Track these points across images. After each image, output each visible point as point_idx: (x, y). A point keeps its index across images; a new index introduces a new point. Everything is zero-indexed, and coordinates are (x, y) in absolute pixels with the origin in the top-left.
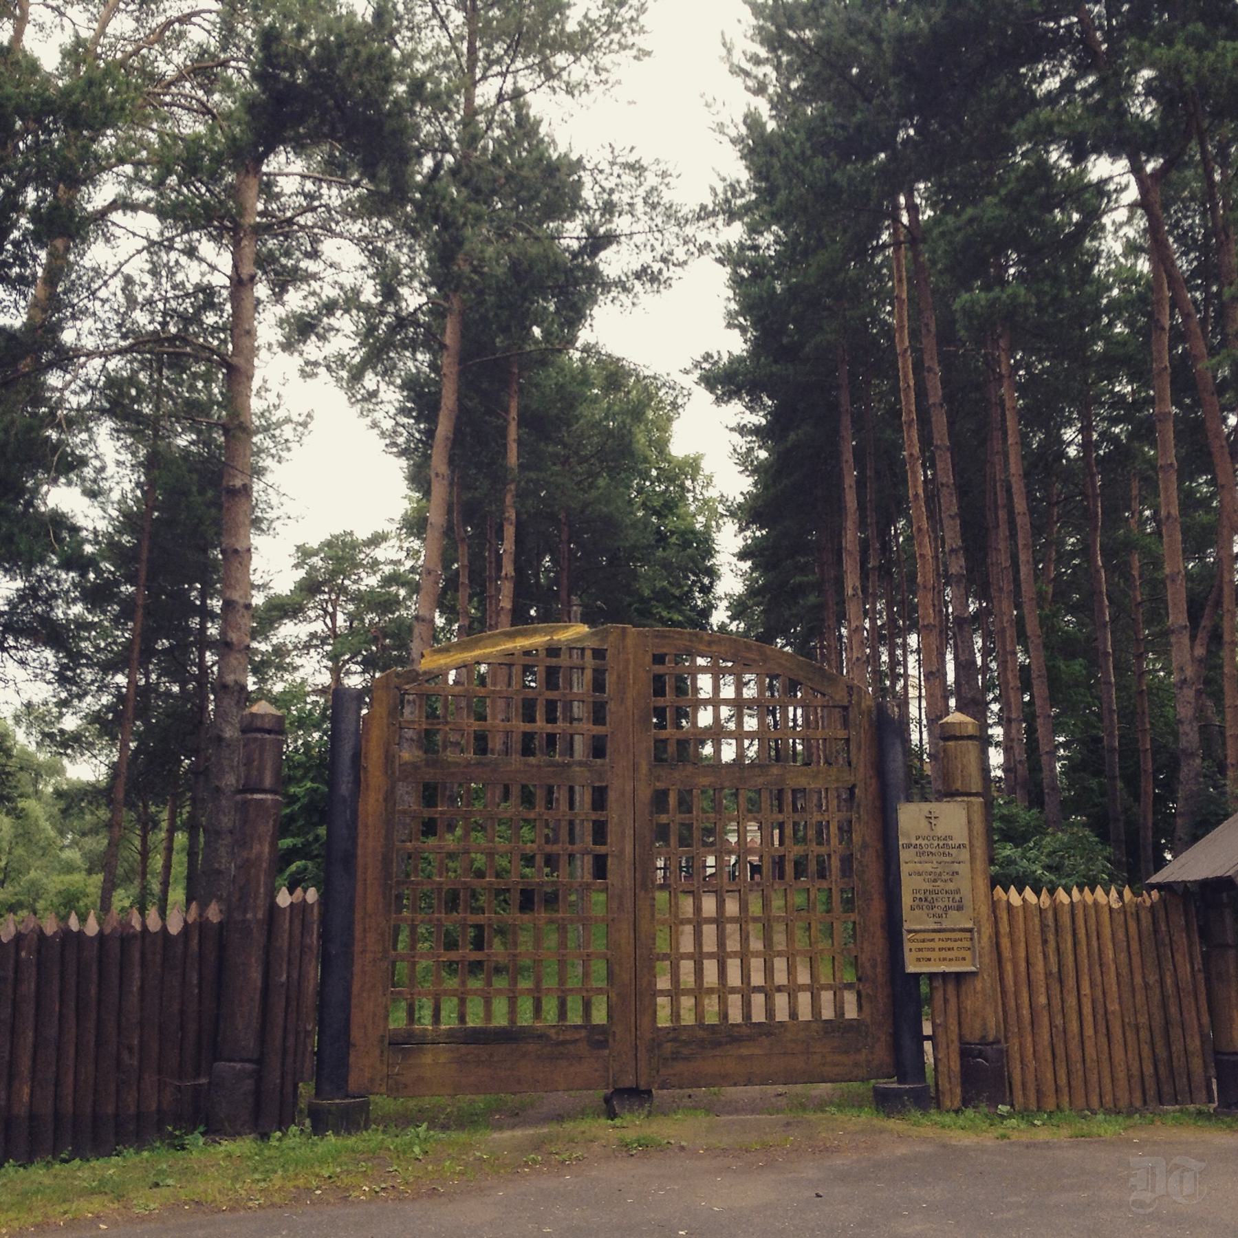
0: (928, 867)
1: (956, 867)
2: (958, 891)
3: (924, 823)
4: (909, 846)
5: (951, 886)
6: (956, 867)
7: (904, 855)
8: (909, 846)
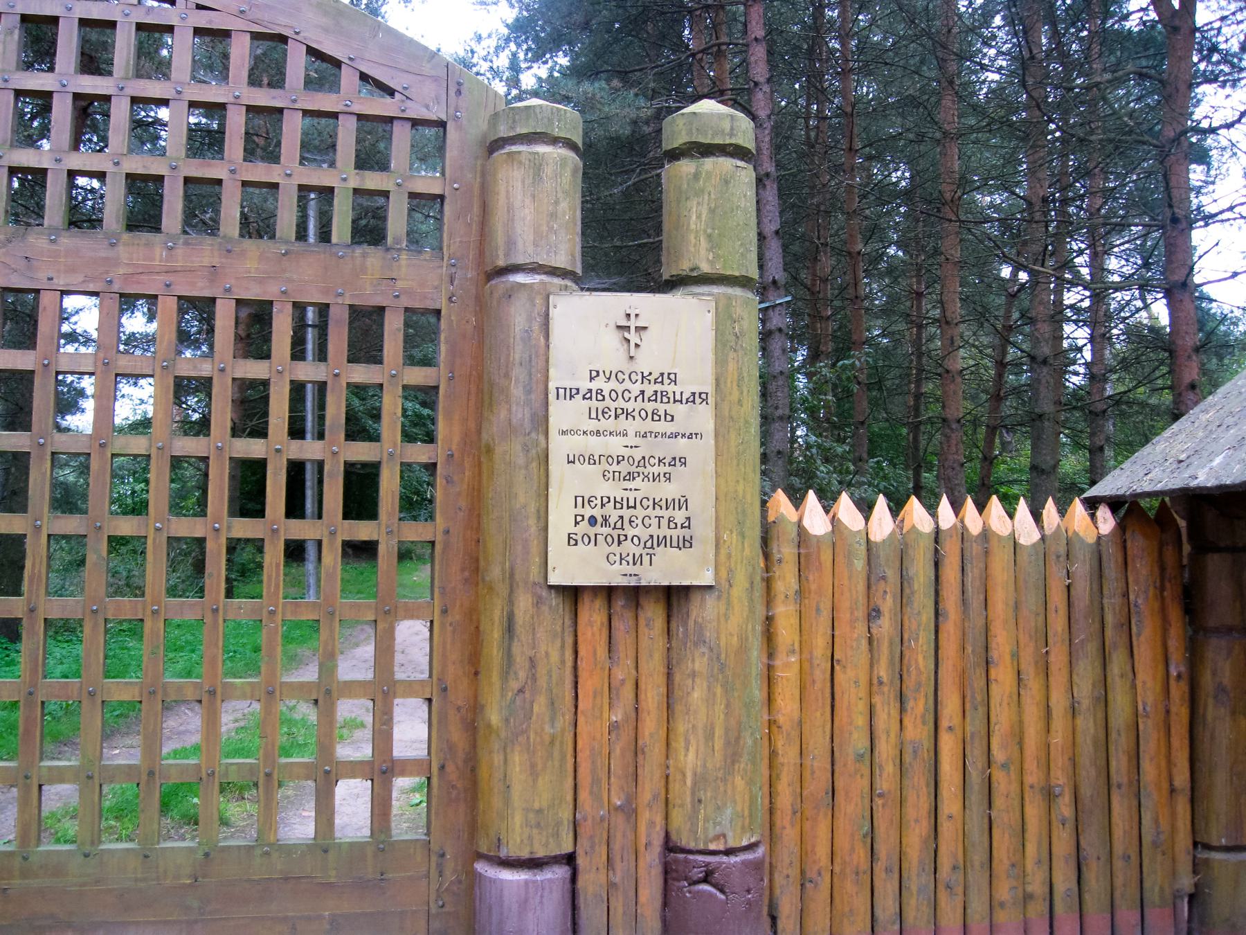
0: (615, 445)
1: (681, 446)
2: (683, 503)
3: (612, 339)
4: (572, 393)
5: (668, 491)
6: (681, 446)
7: (562, 414)
8: (572, 393)
